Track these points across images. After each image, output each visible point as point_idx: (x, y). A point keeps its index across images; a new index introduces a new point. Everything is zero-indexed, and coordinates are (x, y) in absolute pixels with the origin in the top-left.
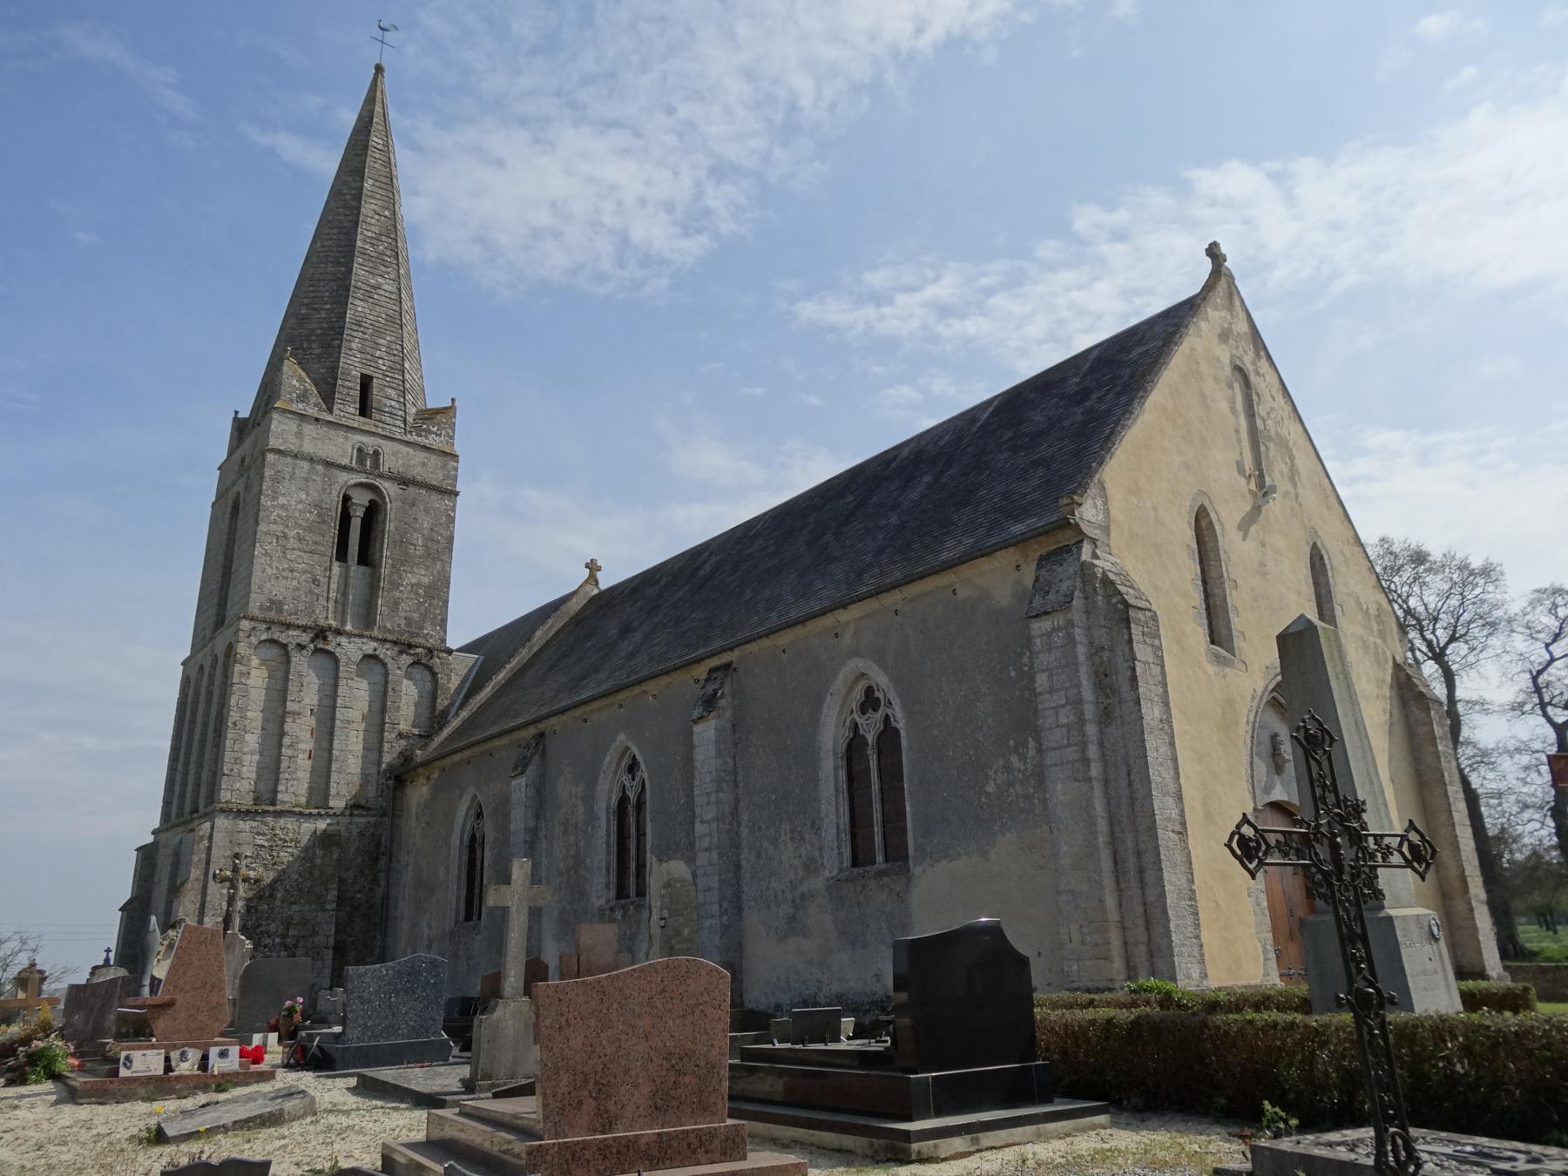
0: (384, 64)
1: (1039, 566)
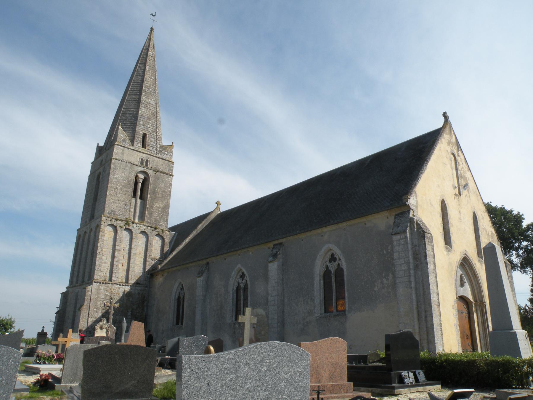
0: (154, 28)
1: (395, 218)
